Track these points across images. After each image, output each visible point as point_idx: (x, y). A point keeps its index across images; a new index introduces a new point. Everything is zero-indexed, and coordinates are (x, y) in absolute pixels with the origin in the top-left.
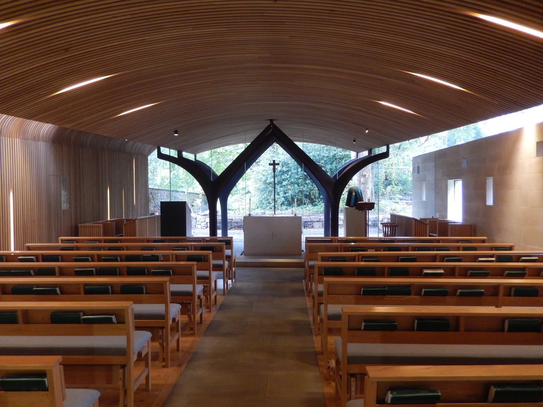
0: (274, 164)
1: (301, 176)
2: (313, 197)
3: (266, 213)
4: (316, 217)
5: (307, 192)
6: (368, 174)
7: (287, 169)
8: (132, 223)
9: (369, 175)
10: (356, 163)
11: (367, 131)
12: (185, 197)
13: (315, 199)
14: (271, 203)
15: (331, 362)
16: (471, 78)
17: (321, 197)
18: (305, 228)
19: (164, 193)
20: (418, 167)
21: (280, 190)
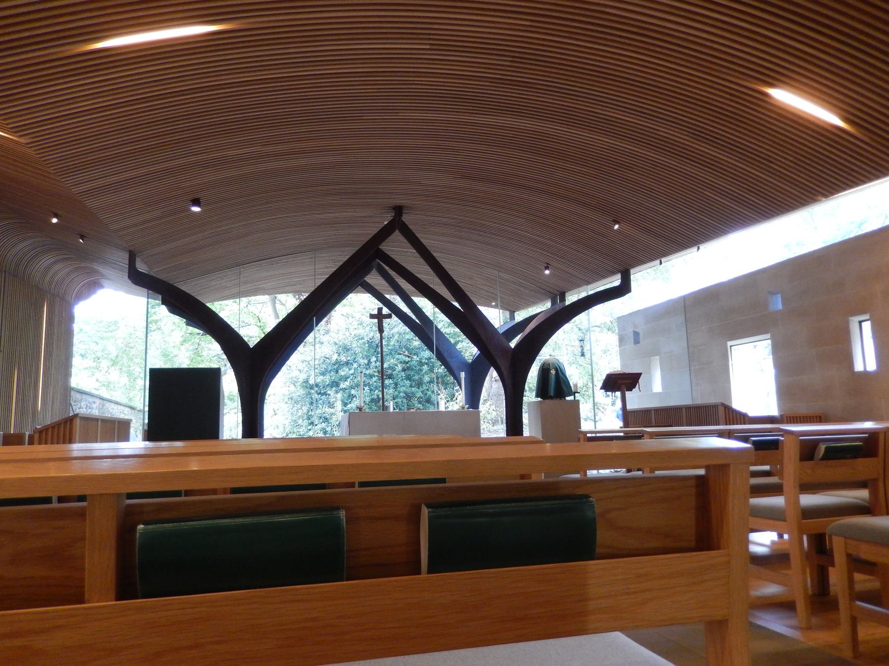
8: (62, 429)
14: (316, 423)
19: (94, 402)
20: (636, 334)
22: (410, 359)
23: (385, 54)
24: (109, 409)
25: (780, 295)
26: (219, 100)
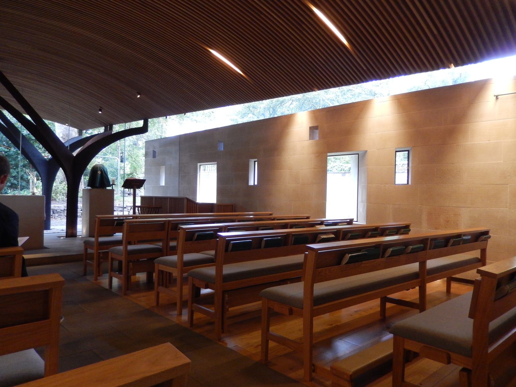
11: (139, 96)
16: (246, 63)
20: (154, 152)
22: (8, 150)
25: (223, 143)
26: (268, 43)
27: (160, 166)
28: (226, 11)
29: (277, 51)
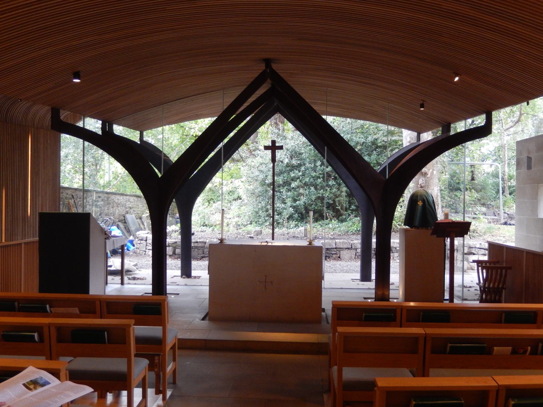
0: (273, 148)
1: (321, 174)
2: (339, 208)
3: (263, 231)
4: (345, 241)
5: (330, 199)
6: (431, 171)
7: (299, 162)
9: (432, 172)
10: (422, 149)
11: (457, 79)
12: (138, 203)
13: (342, 211)
15: (311, 213)
17: (353, 207)
18: (326, 259)
20: (529, 159)
21: (287, 195)
23: (69, 6)
24: (115, 200)
27: (538, 183)
28: (15, 31)
29: (426, 6)
